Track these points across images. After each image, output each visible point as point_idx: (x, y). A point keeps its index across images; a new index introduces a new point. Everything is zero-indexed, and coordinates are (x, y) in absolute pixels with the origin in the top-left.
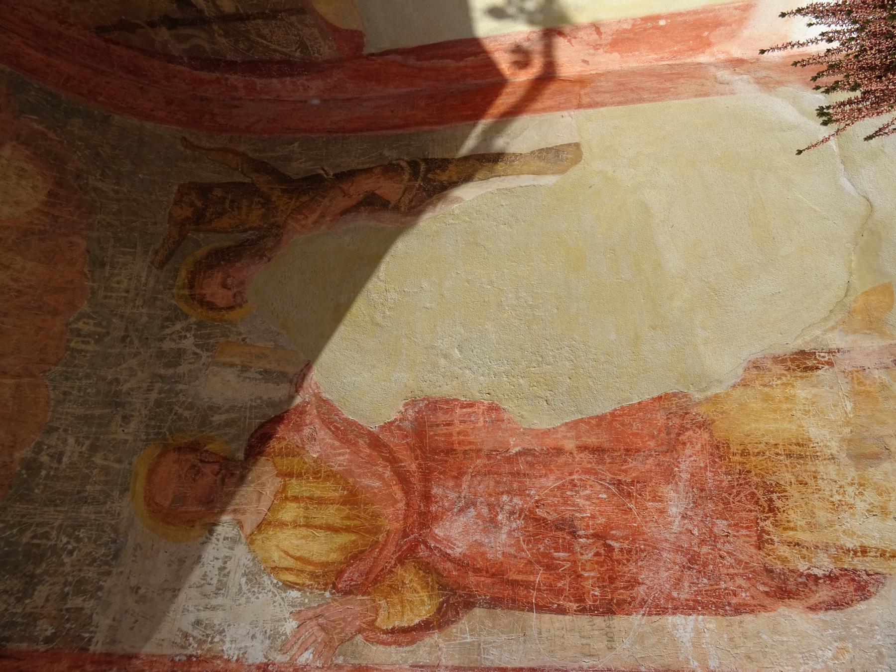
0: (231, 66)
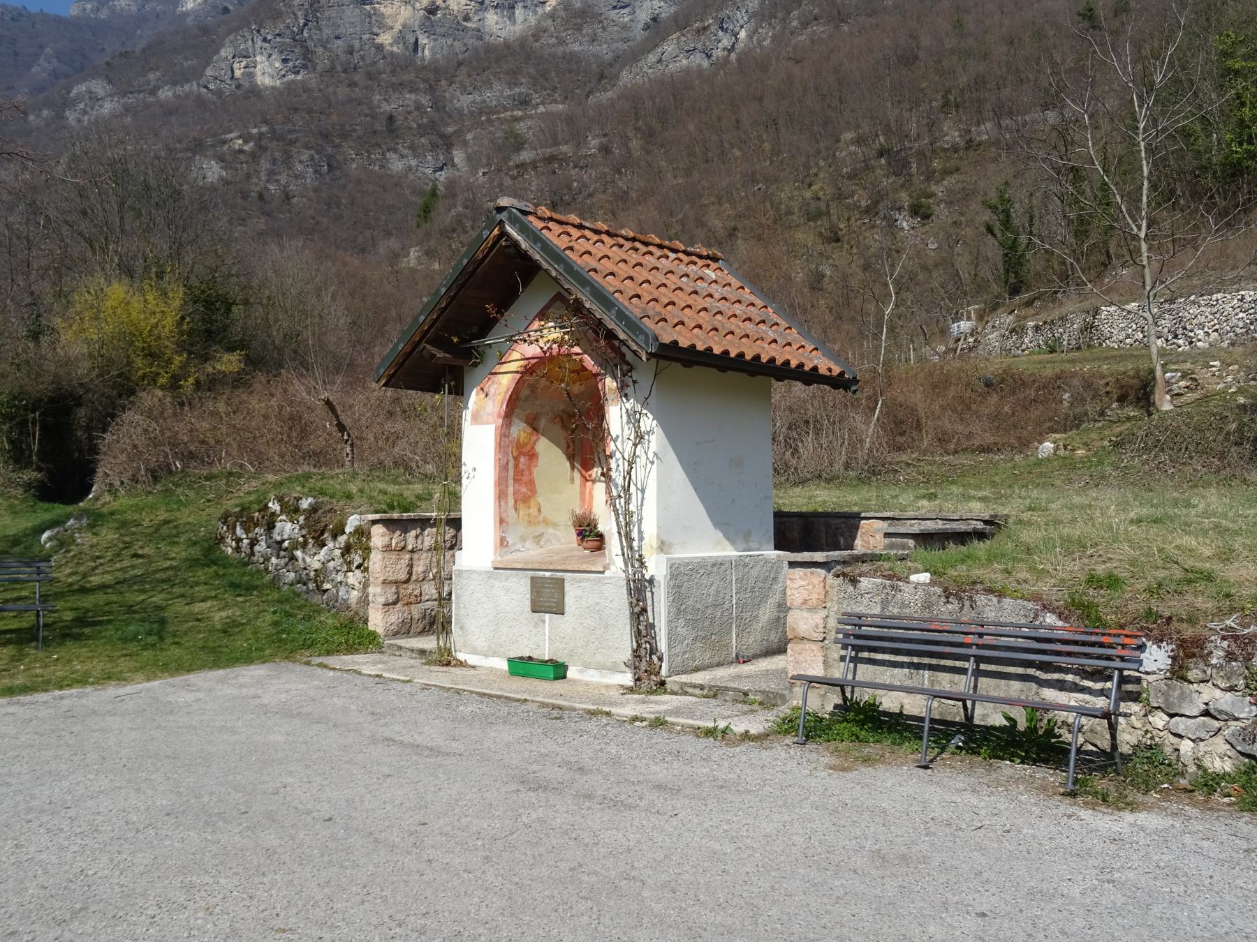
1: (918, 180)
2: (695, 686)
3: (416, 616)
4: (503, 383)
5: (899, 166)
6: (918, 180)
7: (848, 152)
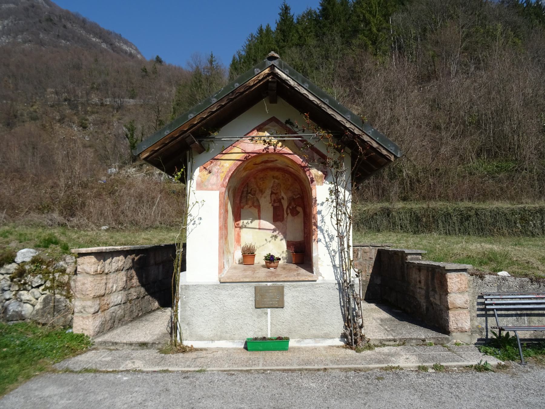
0: (242, 194)
1: (82, 113)
2: (390, 340)
3: (108, 318)
4: (226, 166)
5: (73, 106)
6: (82, 113)
7: (50, 94)
